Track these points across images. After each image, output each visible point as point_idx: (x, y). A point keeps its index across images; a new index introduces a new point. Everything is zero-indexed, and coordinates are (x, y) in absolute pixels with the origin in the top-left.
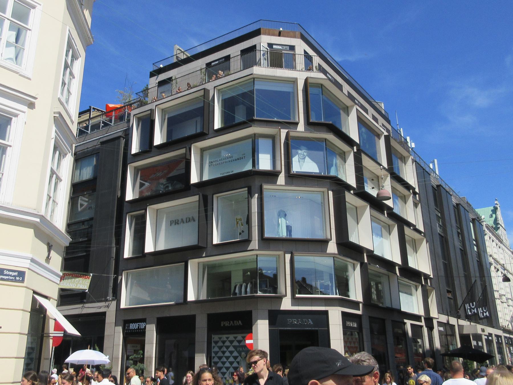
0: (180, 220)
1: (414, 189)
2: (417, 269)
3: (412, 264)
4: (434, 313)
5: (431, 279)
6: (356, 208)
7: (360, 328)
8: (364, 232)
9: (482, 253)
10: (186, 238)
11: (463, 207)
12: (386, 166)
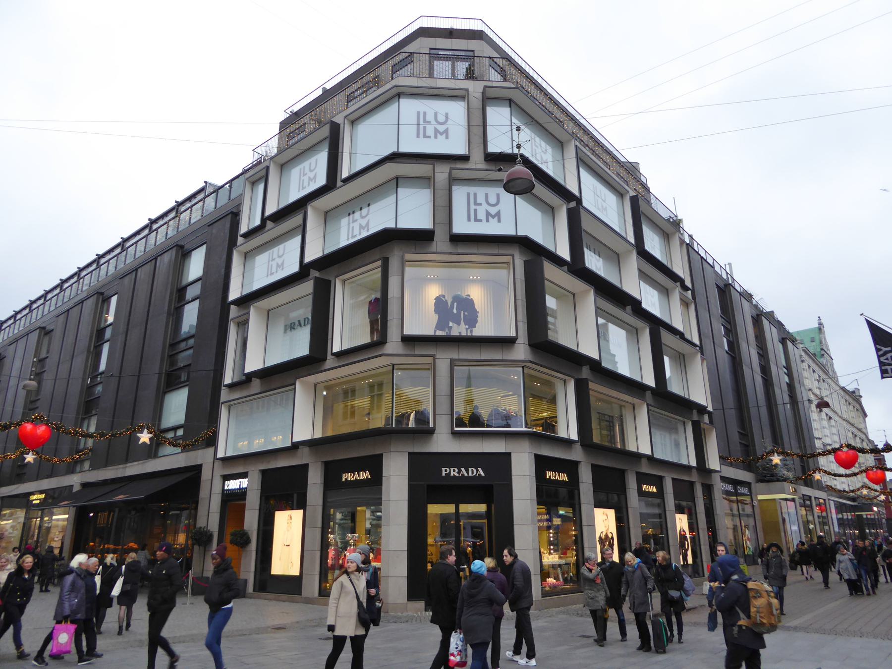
0: (297, 323)
1: (682, 281)
2: (687, 397)
3: (675, 387)
4: (713, 462)
5: (710, 413)
6: (574, 295)
7: (660, 494)
8: (582, 328)
9: (797, 385)
10: (299, 345)
11: (840, 476)
12: (633, 241)
